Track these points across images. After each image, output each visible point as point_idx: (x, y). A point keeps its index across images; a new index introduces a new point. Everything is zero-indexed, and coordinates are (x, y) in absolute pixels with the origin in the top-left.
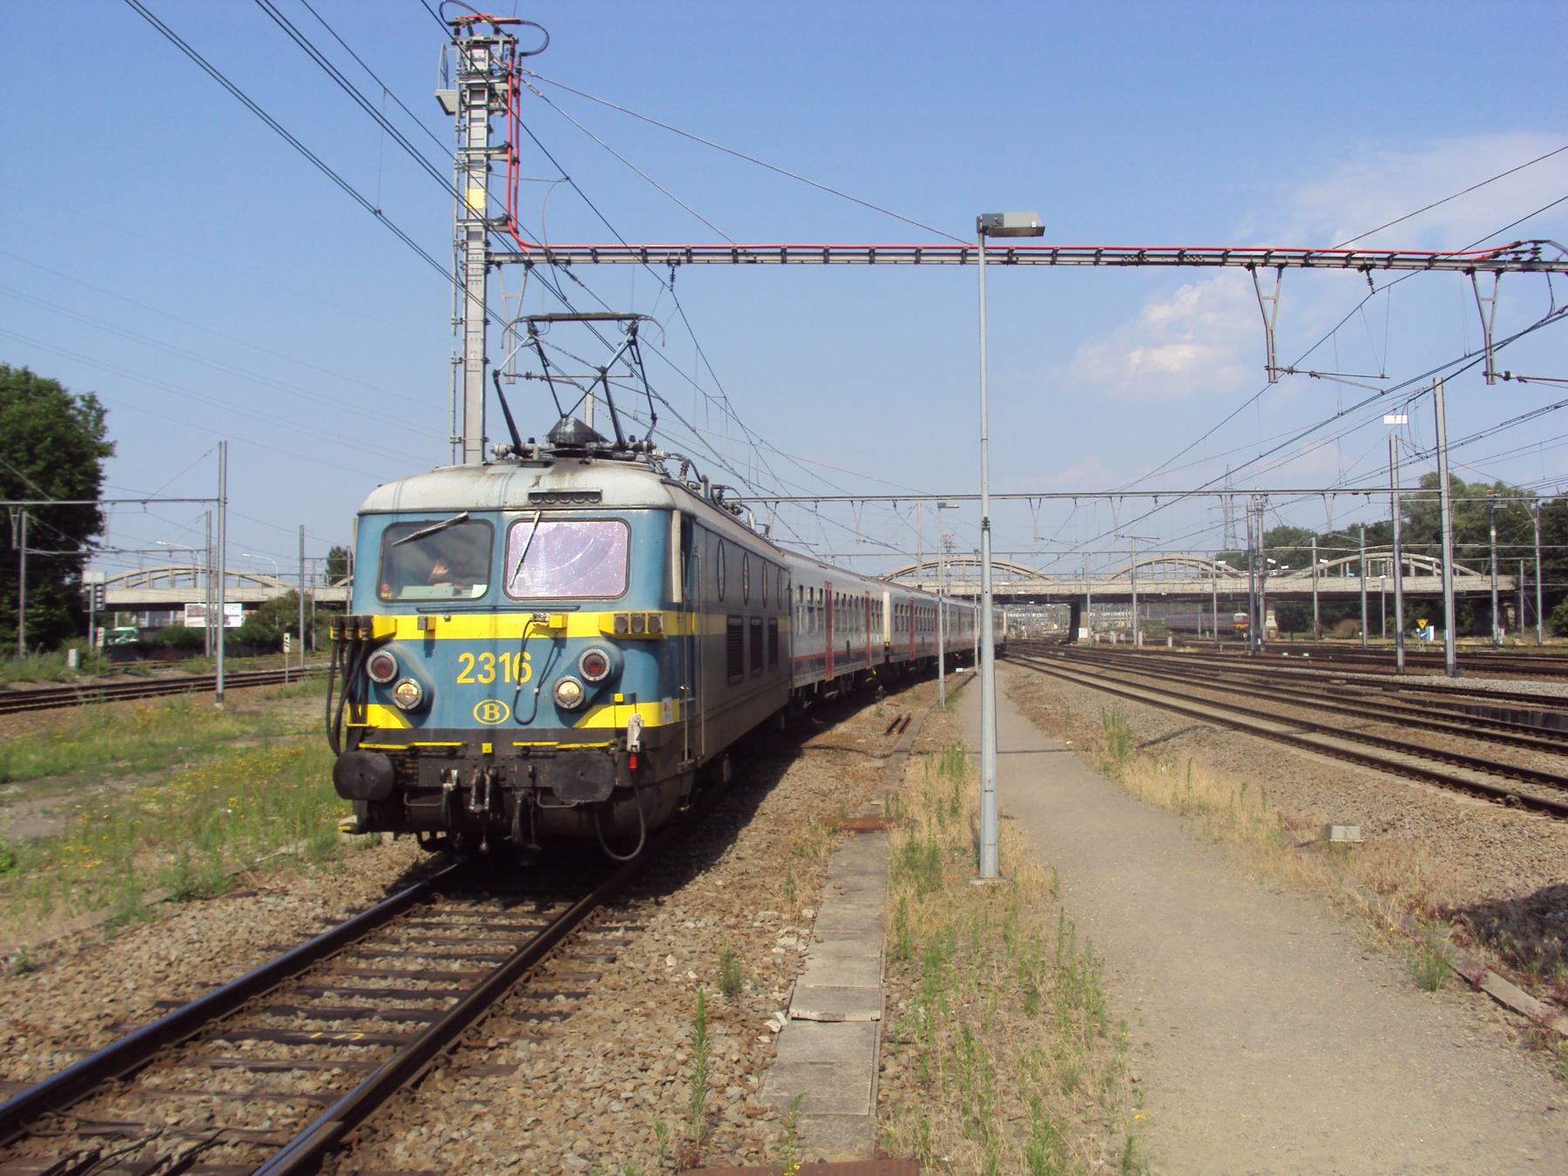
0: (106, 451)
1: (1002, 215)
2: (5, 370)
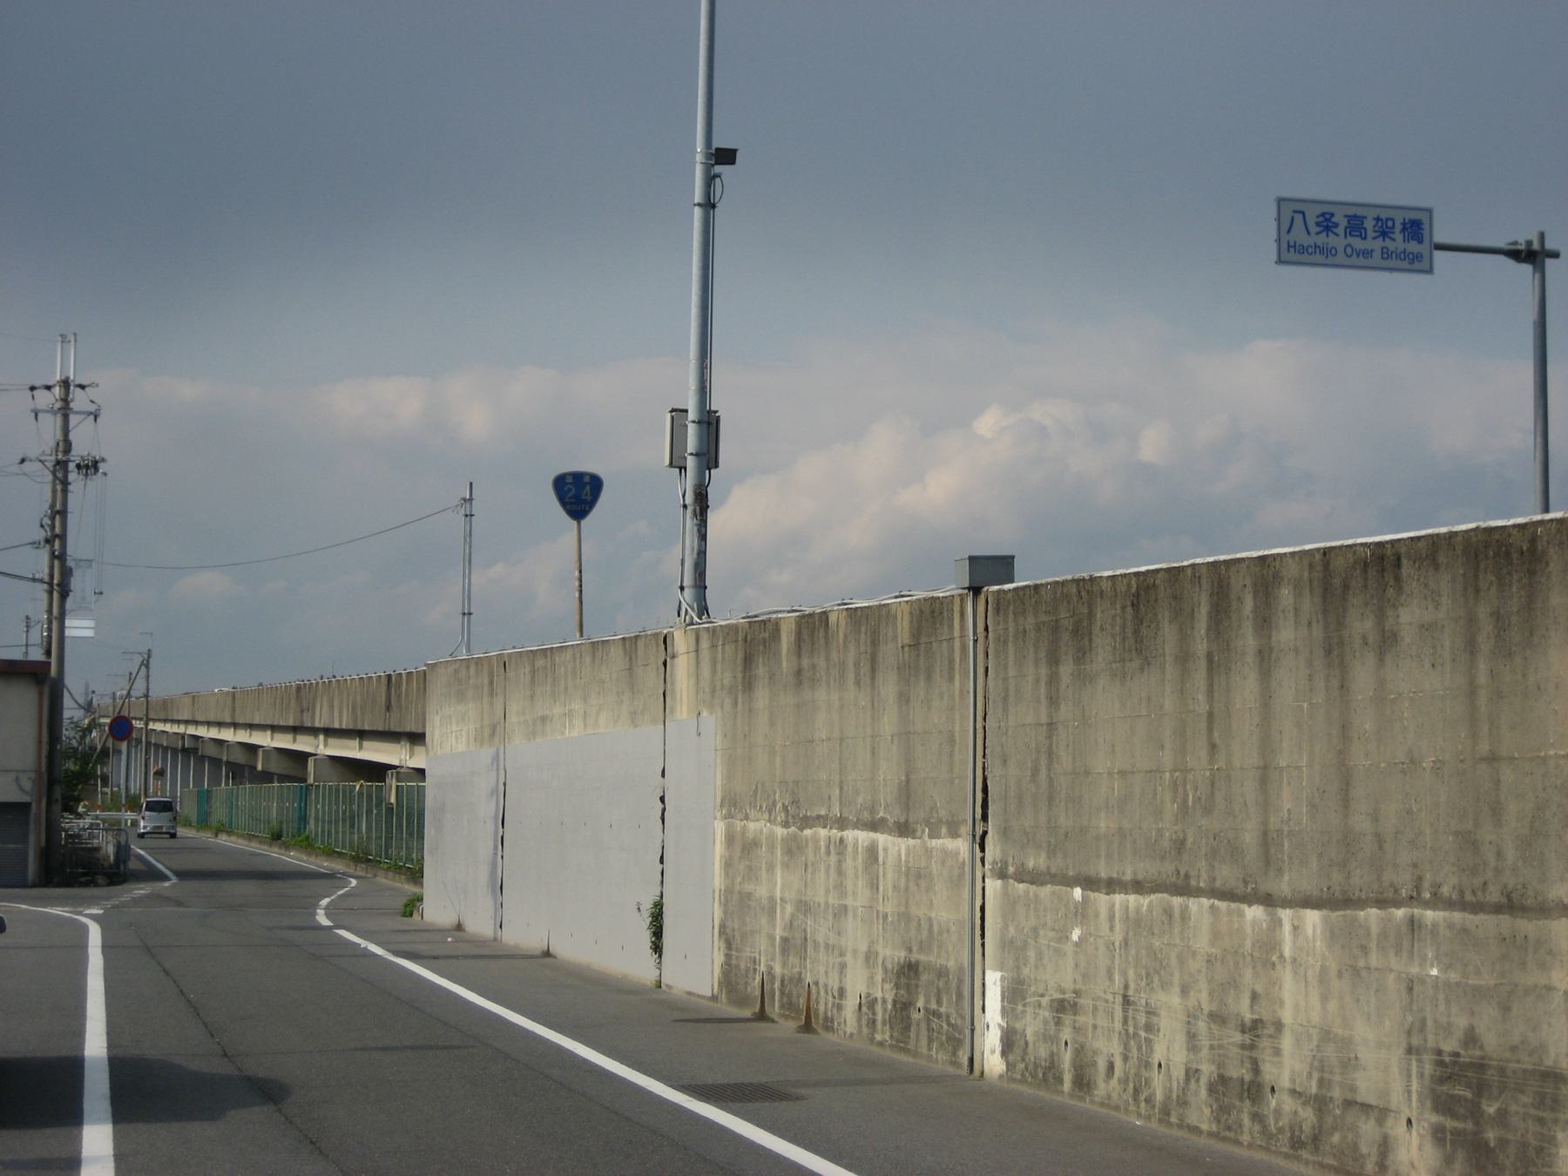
0: (71, 591)
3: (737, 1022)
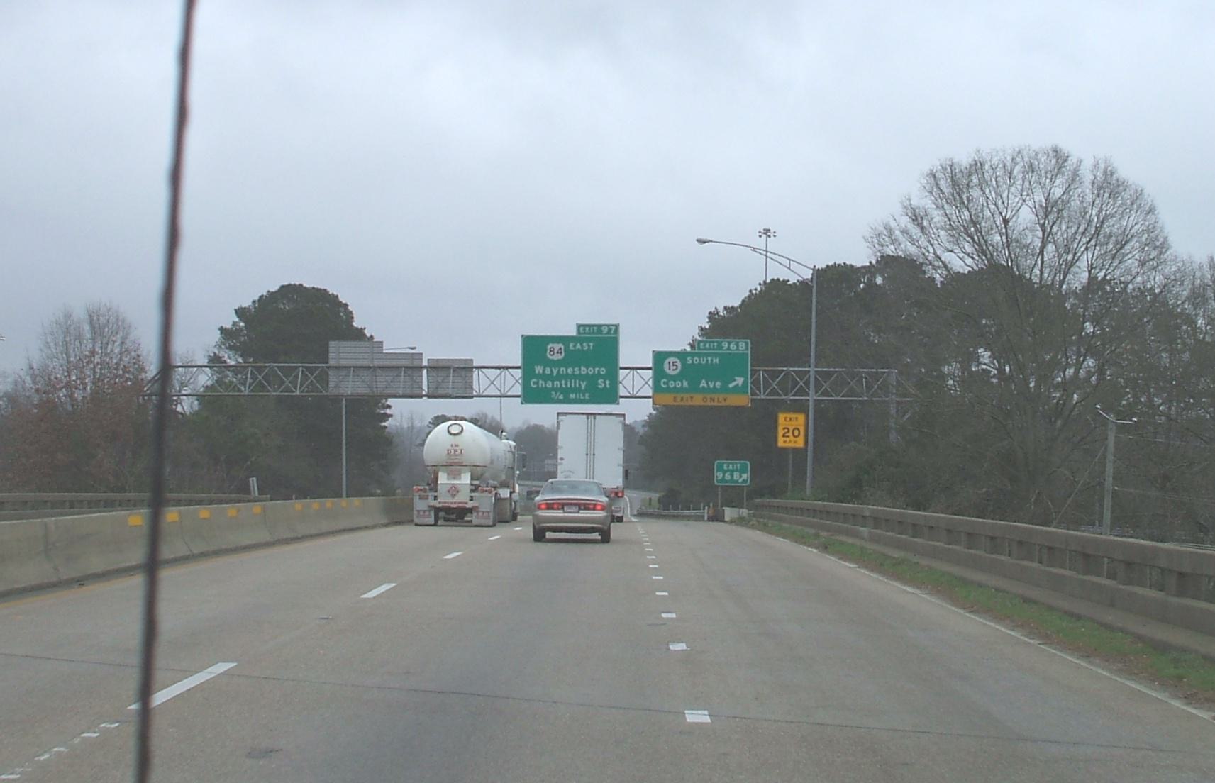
2: (11, 398)
3: (585, 543)
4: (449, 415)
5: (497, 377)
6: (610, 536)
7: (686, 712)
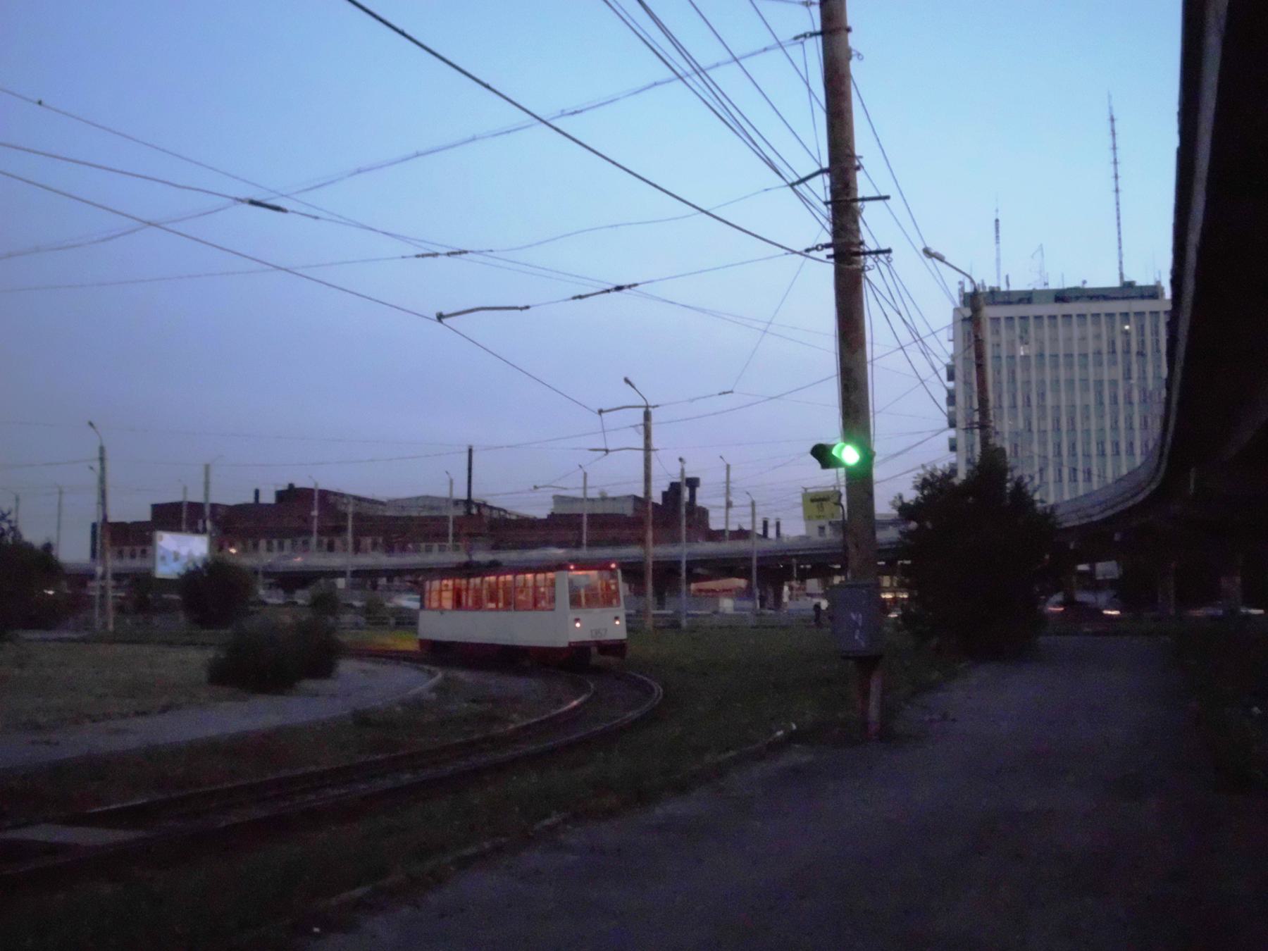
0: (291, 486)
1: (571, 608)
4: (946, 260)
5: (820, 158)
6: (160, 529)
7: (895, 578)
